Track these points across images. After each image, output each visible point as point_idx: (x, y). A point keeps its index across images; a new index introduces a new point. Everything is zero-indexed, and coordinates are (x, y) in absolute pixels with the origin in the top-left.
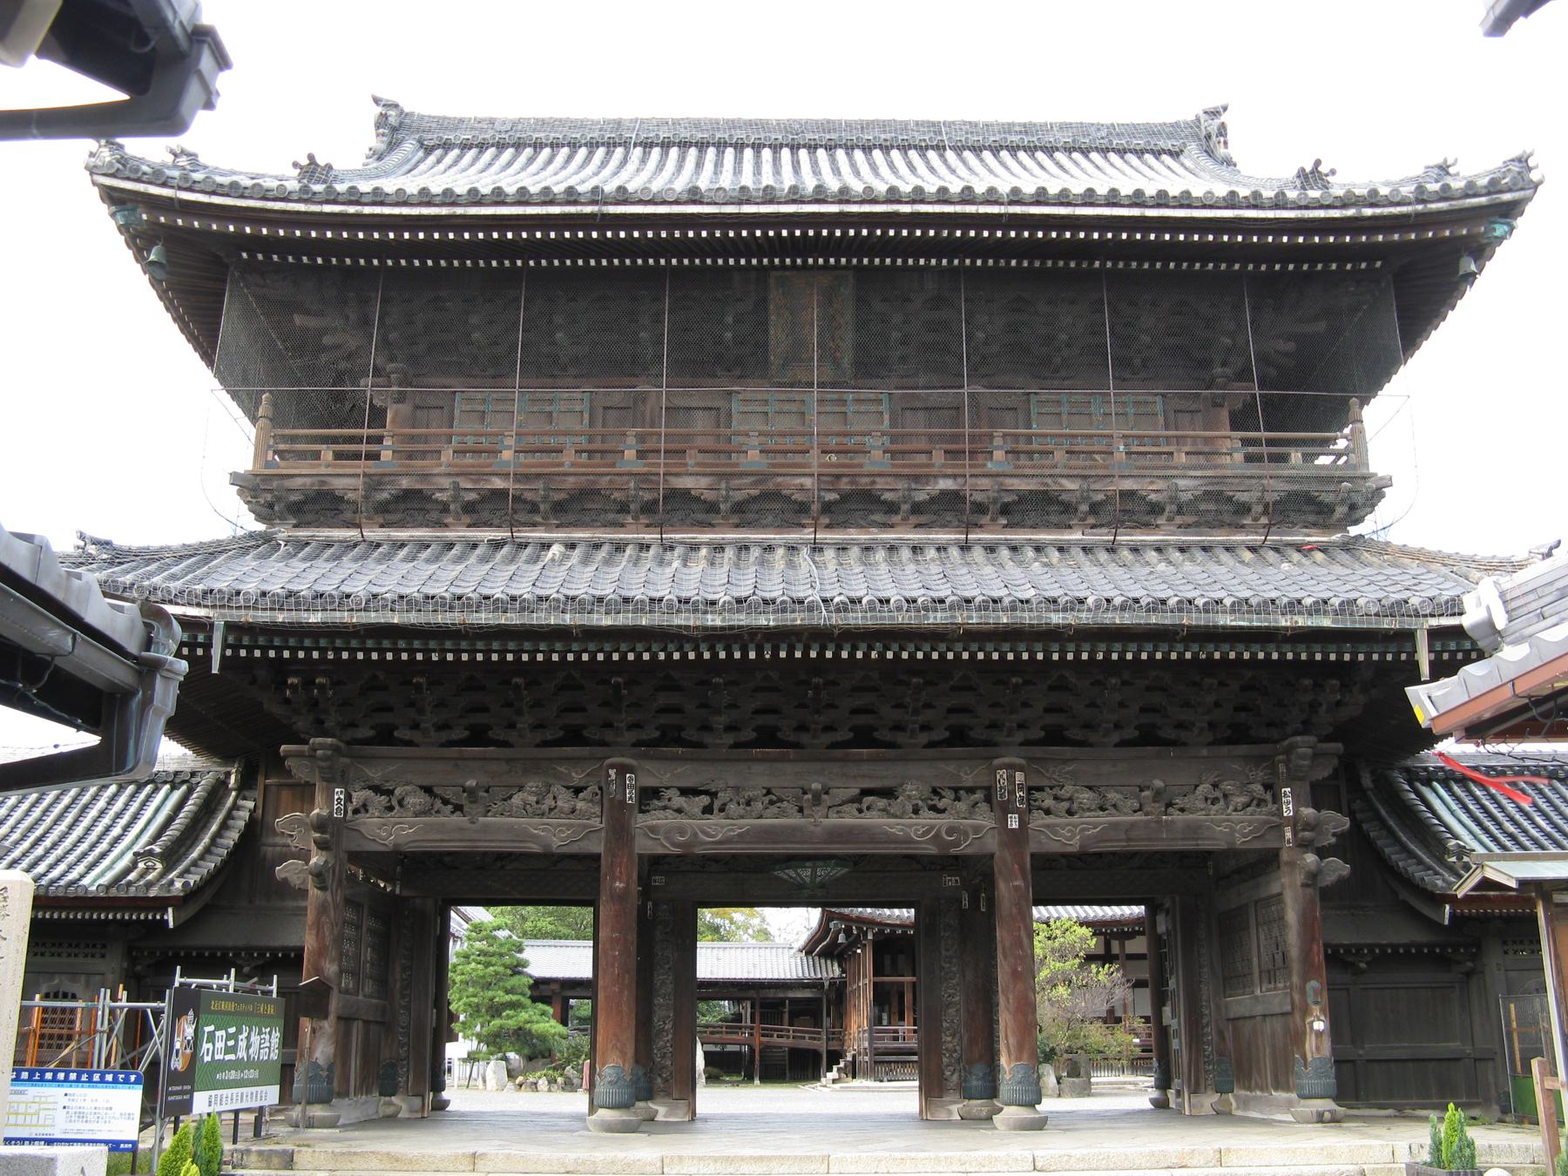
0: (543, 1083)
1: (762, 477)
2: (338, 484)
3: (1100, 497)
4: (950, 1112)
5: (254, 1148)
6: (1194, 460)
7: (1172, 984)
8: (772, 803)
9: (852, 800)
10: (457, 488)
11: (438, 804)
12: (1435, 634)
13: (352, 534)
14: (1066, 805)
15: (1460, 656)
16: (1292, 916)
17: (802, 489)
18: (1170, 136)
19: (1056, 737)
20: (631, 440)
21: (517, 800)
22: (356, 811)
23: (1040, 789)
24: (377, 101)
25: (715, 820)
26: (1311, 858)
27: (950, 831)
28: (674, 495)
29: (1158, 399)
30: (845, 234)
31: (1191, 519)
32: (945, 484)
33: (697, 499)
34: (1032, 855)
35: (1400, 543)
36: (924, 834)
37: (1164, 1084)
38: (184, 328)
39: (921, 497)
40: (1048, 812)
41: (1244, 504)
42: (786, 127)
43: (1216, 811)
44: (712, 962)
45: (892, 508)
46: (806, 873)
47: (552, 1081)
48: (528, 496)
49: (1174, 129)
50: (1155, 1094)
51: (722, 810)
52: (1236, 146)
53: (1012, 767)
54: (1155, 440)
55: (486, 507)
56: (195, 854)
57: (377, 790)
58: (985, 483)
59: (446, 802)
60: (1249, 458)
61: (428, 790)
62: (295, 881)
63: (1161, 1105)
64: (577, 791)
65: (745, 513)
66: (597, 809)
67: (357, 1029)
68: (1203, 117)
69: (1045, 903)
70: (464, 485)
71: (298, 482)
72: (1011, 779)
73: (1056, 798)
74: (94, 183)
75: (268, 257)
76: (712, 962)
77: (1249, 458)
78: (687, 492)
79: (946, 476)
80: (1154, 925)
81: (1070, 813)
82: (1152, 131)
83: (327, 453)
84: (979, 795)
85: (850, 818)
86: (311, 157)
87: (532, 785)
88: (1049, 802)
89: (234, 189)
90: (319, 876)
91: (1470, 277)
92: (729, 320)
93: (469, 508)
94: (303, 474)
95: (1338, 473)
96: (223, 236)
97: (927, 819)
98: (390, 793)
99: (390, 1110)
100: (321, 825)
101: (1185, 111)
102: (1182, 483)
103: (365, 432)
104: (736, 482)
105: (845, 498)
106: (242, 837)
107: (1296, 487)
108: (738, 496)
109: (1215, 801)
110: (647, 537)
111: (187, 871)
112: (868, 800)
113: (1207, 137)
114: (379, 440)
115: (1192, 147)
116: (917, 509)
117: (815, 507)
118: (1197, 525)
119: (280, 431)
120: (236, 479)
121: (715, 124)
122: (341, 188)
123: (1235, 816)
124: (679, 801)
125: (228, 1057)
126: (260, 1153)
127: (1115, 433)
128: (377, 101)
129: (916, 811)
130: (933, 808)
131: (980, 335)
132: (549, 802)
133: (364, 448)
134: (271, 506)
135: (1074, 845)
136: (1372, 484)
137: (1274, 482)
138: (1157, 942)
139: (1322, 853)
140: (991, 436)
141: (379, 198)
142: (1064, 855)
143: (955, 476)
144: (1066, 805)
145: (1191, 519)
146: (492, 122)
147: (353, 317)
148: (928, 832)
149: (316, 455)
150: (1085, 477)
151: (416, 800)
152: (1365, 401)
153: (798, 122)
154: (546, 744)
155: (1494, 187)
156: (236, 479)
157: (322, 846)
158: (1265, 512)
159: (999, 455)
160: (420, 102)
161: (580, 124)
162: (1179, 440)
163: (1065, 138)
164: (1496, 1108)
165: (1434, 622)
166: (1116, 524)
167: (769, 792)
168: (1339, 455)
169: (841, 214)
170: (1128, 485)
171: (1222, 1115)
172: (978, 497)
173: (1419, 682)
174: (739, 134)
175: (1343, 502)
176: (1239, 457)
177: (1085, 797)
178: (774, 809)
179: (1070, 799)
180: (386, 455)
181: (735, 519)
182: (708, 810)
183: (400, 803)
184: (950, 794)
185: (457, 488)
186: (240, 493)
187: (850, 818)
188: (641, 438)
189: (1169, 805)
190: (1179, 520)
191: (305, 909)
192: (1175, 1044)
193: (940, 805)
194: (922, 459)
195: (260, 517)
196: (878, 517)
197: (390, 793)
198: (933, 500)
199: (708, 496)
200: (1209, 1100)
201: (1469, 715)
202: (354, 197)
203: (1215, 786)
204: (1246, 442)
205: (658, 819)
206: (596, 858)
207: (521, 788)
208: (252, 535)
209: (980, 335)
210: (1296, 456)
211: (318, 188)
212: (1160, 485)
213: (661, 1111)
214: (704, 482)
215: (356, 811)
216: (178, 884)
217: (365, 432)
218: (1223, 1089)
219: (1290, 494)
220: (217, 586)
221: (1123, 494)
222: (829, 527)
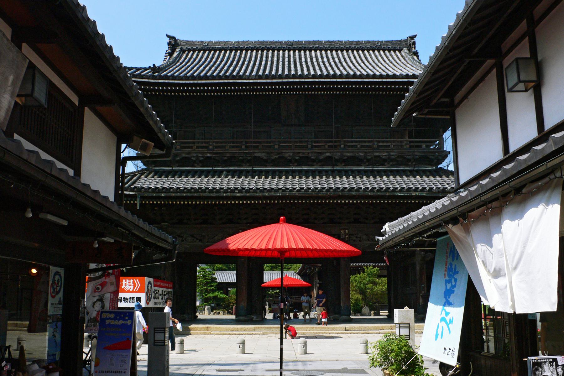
0: (221, 312)
1: (279, 153)
3: (369, 157)
11: (195, 240)
16: (418, 268)
17: (290, 156)
18: (399, 45)
19: (356, 221)
20: (244, 143)
23: (352, 235)
24: (168, 36)
31: (394, 163)
32: (328, 154)
33: (262, 159)
39: (322, 158)
42: (287, 43)
45: (314, 161)
47: (224, 312)
48: (217, 158)
49: (401, 42)
53: (345, 229)
56: (445, 201)
61: (193, 236)
68: (409, 39)
70: (200, 155)
72: (345, 232)
73: (356, 237)
79: (328, 152)
81: (360, 241)
82: (393, 43)
86: (154, 65)
88: (355, 238)
92: (270, 108)
98: (182, 237)
101: (403, 36)
102: (392, 154)
108: (273, 158)
115: (405, 49)
117: (293, 161)
121: (266, 42)
125: (116, 323)
128: (168, 36)
136: (444, 154)
143: (330, 152)
145: (394, 163)
146: (202, 42)
150: (365, 152)
151: (190, 239)
153: (290, 41)
154: (224, 223)
160: (180, 37)
161: (226, 43)
163: (368, 46)
169: (300, 82)
174: (274, 46)
176: (408, 146)
177: (364, 237)
179: (360, 238)
185: (197, 156)
190: (391, 163)
196: (310, 163)
197: (182, 237)
199: (265, 158)
208: (143, 170)
212: (386, 154)
214: (263, 154)
220: (137, 186)
222: (296, 166)
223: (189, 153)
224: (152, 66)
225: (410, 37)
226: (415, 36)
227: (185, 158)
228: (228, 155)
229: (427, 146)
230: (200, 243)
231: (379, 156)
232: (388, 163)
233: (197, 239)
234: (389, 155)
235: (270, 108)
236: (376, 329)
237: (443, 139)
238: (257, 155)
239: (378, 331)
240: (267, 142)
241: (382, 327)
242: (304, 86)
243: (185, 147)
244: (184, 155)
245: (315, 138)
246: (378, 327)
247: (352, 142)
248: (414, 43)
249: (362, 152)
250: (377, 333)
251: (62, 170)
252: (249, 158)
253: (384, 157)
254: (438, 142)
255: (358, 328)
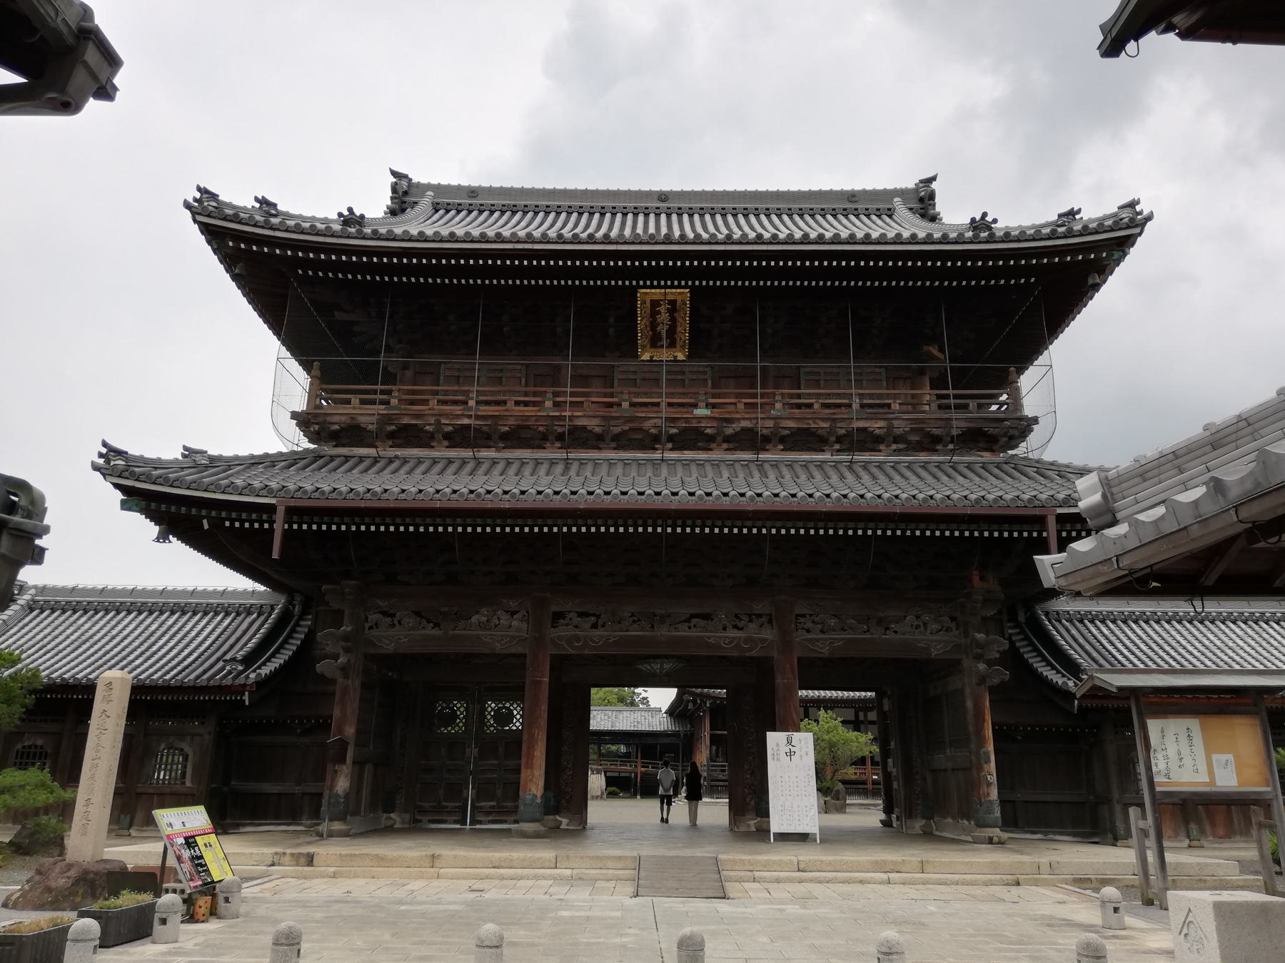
1: (630, 419)
2: (362, 419)
4: (749, 826)
5: (288, 851)
6: (905, 408)
7: (893, 745)
8: (634, 622)
9: (685, 621)
10: (438, 423)
11: (424, 621)
12: (1061, 519)
13: (372, 451)
14: (820, 627)
15: (1074, 534)
20: (550, 395)
21: (474, 619)
22: (371, 628)
25: (598, 632)
26: (982, 666)
27: (747, 640)
28: (574, 430)
29: (883, 370)
30: (683, 264)
34: (799, 659)
35: (1050, 460)
36: (730, 643)
37: (888, 810)
38: (261, 315)
39: (729, 431)
40: (808, 631)
41: (937, 436)
43: (921, 633)
44: (601, 720)
45: (711, 439)
46: (657, 667)
48: (485, 428)
50: (883, 816)
51: (603, 626)
52: (940, 206)
54: (880, 396)
55: (460, 437)
57: (385, 614)
58: (770, 424)
59: (429, 621)
60: (940, 407)
61: (418, 614)
62: (328, 674)
63: (887, 824)
64: (513, 613)
65: (621, 442)
66: (525, 626)
67: (368, 768)
69: (806, 689)
70: (444, 421)
71: (336, 419)
74: (195, 221)
75: (315, 273)
76: (601, 720)
77: (940, 407)
78: (584, 428)
80: (880, 705)
81: (822, 632)
83: (355, 400)
84: (764, 619)
85: (684, 632)
87: (484, 610)
88: (809, 625)
89: (298, 229)
90: (344, 670)
91: (1096, 287)
92: (612, 320)
93: (447, 436)
94: (339, 414)
95: (1003, 416)
96: (283, 257)
97: (732, 633)
98: (392, 616)
99: (390, 822)
100: (346, 638)
102: (896, 423)
103: (379, 387)
104: (612, 422)
105: (683, 431)
106: (303, 642)
107: (973, 425)
108: (617, 430)
109: (918, 627)
110: (558, 455)
111: (259, 668)
112: (694, 621)
113: (923, 200)
114: (389, 392)
116: (727, 439)
117: (664, 438)
118: (907, 449)
119: (324, 386)
120: (295, 415)
122: (368, 231)
123: (931, 637)
124: (577, 620)
126: (292, 855)
127: (853, 391)
129: (724, 629)
130: (735, 627)
131: (769, 330)
132: (495, 621)
133: (379, 397)
134: (318, 433)
135: (825, 651)
137: (959, 422)
138: (883, 715)
139: (990, 663)
140: (774, 394)
141: (391, 237)
142: (821, 659)
143: (750, 419)
144: (820, 627)
145: (901, 446)
147: (374, 314)
148: (730, 643)
149: (348, 402)
150: (834, 420)
151: (410, 621)
152: (1021, 371)
155: (1117, 226)
156: (295, 415)
157: (347, 650)
158: (952, 442)
159: (778, 406)
162: (895, 397)
164: (1110, 836)
165: (1060, 511)
166: (850, 450)
167: (633, 615)
168: (1001, 404)
170: (862, 424)
171: (928, 836)
172: (765, 431)
173: (1047, 552)
175: (1005, 435)
176: (934, 406)
177: (833, 622)
178: (636, 626)
180: (394, 402)
181: (614, 445)
182: (594, 626)
183: (400, 622)
184: (746, 618)
185: (438, 423)
186: (297, 425)
187: (684, 632)
188: (556, 394)
189: (887, 629)
190: (894, 447)
191: (333, 694)
192: (895, 785)
193: (740, 624)
194: (731, 408)
195: (311, 441)
198: (737, 434)
199: (597, 430)
200: (918, 824)
201: (1110, 573)
202: (376, 235)
203: (918, 617)
204: (939, 397)
205: (563, 631)
206: (525, 656)
207: (477, 613)
209: (769, 330)
210: (972, 404)
211: (352, 230)
212: (881, 424)
213: (564, 823)
214: (594, 422)
215: (371, 628)
216: (253, 676)
217: (379, 387)
218: (928, 817)
219: (969, 429)
221: (858, 429)
223: (418, 416)
224: (346, 213)
225: (921, 181)
226: (934, 179)
227: (407, 427)
228: (511, 422)
229: (980, 406)
230: (436, 632)
231: (865, 429)
232: (888, 446)
233: (429, 621)
234: (890, 427)
235: (612, 320)
236: (879, 867)
237: (1018, 389)
238: (579, 422)
239: (884, 876)
240: (605, 395)
241: (894, 863)
242: (691, 263)
243: (412, 403)
244: (406, 421)
245: (713, 387)
246: (885, 862)
247: (799, 396)
248: (932, 196)
249: (824, 420)
250: (882, 883)
251: (538, 684)
252: (560, 430)
253: (877, 431)
254: (1004, 397)
255: (830, 864)
